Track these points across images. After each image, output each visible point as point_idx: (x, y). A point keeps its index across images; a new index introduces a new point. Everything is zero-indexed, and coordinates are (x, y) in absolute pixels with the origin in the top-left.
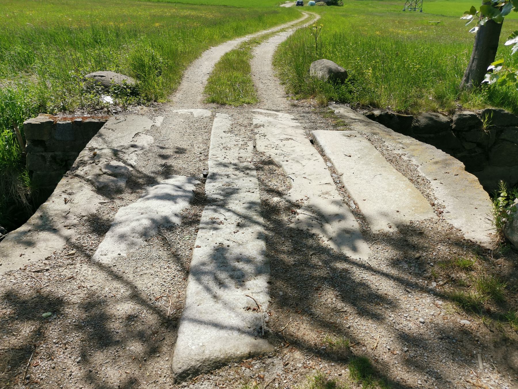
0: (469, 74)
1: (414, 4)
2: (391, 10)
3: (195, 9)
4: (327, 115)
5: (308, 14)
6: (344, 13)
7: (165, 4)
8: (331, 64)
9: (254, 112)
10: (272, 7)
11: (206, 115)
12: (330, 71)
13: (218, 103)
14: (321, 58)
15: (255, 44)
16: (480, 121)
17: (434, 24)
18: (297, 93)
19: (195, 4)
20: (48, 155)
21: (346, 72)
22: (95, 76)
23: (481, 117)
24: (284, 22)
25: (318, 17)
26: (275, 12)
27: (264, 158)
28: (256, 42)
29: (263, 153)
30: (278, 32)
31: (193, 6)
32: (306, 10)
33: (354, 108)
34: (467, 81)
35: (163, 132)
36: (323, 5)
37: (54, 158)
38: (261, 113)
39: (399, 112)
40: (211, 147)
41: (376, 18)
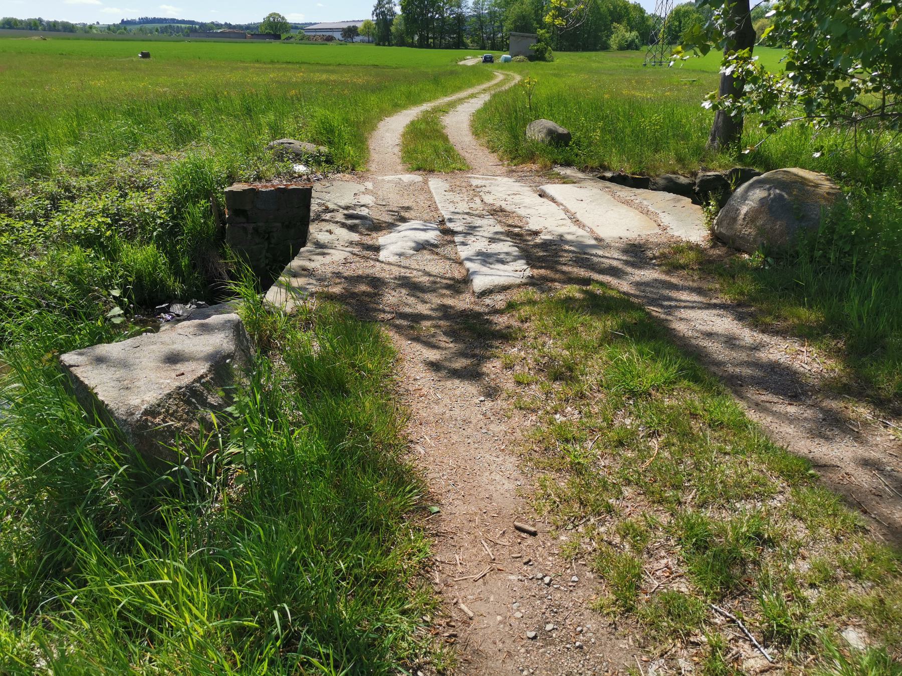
0: (715, 131)
1: (658, 56)
2: (625, 66)
3: (333, 72)
4: (553, 176)
5: (503, 74)
6: (556, 72)
7: (284, 66)
8: (549, 123)
9: (470, 177)
10: (447, 65)
11: (416, 181)
12: (551, 132)
13: (425, 170)
14: (537, 118)
15: (441, 113)
16: (726, 182)
17: (688, 83)
18: (514, 159)
19: (329, 65)
20: (250, 227)
21: (569, 133)
22: (282, 143)
23: (728, 178)
24: (472, 85)
25: (518, 78)
26: (452, 73)
27: (495, 208)
28: (444, 110)
29: (493, 205)
30: (467, 98)
31: (327, 68)
32: (499, 68)
33: (583, 170)
34: (713, 140)
35: (380, 193)
36: (523, 61)
37: (256, 230)
38: (477, 178)
39: (633, 174)
40: (437, 202)
41: (604, 77)
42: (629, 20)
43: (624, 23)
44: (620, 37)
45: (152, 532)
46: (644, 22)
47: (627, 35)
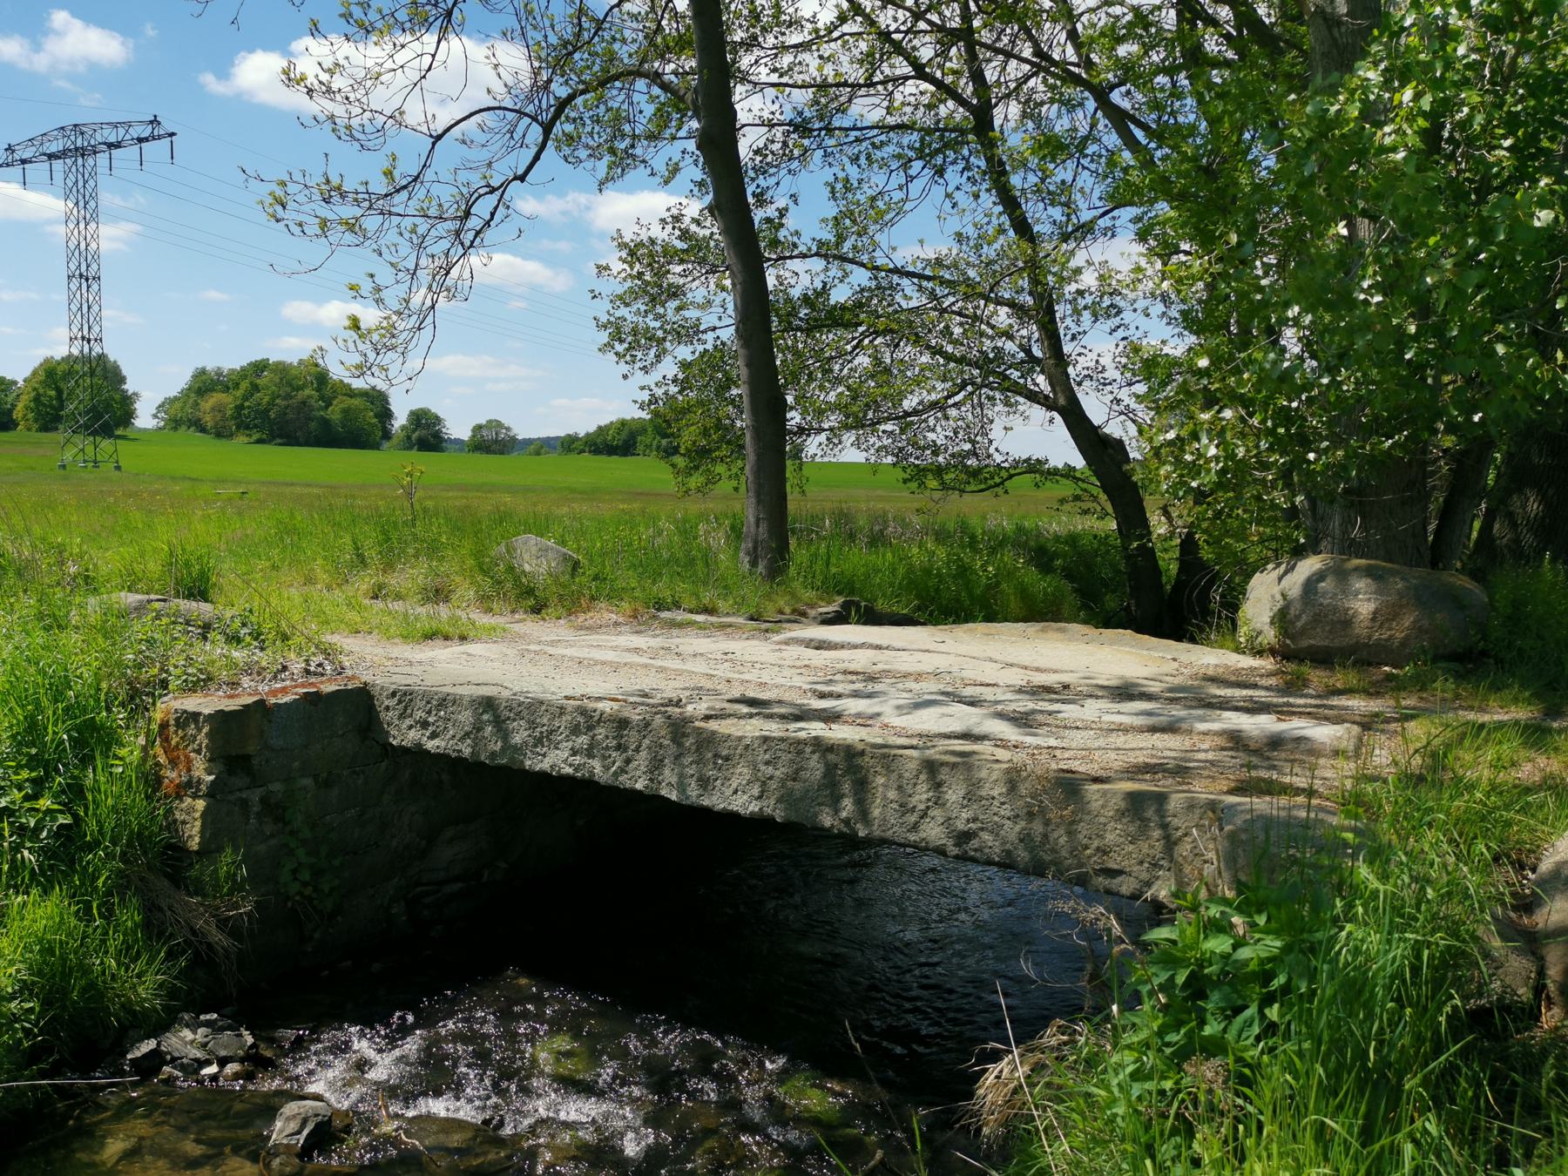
20: (255, 796)
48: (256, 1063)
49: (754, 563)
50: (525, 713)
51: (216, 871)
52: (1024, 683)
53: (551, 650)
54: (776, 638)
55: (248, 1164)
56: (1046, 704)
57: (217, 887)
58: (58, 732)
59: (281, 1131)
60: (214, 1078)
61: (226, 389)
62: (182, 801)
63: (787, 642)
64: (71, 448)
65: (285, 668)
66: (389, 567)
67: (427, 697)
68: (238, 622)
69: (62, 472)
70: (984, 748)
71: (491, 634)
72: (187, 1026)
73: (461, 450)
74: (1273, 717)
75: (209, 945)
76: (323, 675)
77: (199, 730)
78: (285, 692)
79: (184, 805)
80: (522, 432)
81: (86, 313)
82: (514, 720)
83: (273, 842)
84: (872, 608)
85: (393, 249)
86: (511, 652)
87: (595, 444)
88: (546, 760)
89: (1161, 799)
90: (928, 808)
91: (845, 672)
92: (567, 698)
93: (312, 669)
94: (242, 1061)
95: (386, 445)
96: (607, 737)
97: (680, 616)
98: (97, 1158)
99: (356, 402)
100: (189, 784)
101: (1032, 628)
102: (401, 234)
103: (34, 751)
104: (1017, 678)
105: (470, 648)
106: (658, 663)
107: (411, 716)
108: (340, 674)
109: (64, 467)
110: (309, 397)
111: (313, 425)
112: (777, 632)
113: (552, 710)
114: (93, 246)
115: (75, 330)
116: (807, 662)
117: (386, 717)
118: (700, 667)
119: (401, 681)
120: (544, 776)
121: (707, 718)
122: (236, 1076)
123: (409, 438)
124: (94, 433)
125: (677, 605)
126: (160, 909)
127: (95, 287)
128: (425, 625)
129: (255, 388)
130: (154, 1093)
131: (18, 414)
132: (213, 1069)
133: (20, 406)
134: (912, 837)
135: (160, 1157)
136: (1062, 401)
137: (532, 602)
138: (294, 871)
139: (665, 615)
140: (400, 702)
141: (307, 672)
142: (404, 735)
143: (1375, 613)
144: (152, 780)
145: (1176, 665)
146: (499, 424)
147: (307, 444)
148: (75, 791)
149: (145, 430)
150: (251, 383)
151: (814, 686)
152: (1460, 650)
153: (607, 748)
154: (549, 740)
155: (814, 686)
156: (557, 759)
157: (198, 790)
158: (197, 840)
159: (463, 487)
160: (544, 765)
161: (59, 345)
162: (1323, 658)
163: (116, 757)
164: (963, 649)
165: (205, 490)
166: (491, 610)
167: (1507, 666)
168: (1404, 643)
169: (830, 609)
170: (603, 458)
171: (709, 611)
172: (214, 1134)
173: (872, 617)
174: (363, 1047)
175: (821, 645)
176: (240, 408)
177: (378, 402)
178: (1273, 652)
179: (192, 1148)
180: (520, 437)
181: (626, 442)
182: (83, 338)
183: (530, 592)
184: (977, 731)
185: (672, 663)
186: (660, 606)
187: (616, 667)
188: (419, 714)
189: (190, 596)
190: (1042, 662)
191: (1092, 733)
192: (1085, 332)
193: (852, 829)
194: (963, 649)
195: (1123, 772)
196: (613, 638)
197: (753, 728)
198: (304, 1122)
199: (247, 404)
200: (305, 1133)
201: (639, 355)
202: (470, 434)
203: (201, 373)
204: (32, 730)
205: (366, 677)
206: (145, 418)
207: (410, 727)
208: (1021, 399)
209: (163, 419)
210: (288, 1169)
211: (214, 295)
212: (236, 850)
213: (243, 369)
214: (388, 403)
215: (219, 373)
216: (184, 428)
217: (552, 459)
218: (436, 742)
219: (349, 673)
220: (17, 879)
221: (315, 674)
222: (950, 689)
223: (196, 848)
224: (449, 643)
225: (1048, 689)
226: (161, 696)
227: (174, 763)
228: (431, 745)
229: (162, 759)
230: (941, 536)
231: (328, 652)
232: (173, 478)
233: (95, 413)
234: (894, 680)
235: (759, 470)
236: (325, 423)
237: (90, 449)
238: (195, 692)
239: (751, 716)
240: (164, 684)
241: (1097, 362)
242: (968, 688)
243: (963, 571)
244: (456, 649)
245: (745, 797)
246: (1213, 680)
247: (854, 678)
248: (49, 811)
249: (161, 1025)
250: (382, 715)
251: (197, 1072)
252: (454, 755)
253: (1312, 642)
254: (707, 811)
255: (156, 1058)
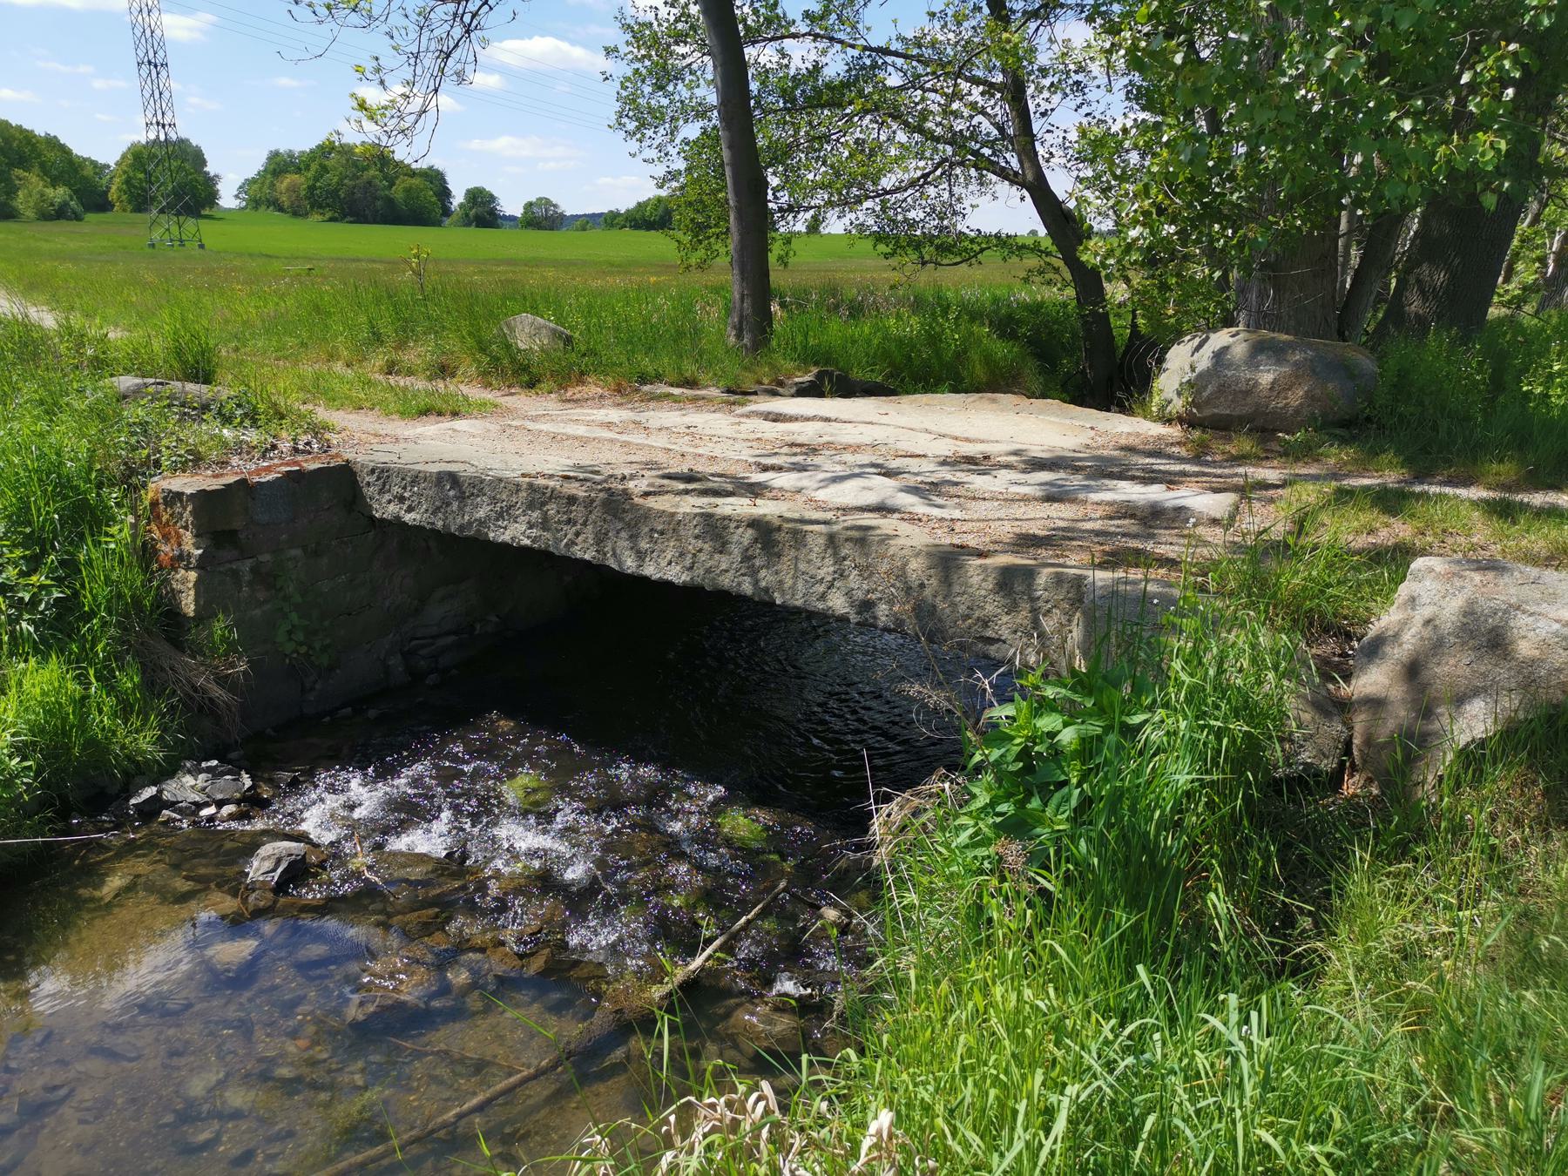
20: (246, 566)
42: (42, 165)
43: (36, 169)
44: (36, 197)
45: (1207, 996)
46: (76, 171)
47: (50, 192)
48: (253, 803)
49: (739, 336)
50: (487, 489)
51: (211, 634)
52: (950, 454)
53: (530, 425)
54: (740, 410)
55: (229, 898)
56: (963, 474)
57: (214, 649)
58: (47, 513)
59: (258, 870)
60: (211, 819)
61: (298, 170)
62: (177, 572)
63: (748, 416)
64: (162, 228)
65: (274, 447)
66: (401, 345)
67: (403, 475)
68: (232, 404)
69: (150, 250)
70: (887, 524)
71: (483, 409)
72: (189, 772)
73: (516, 227)
74: (1163, 487)
75: (211, 699)
76: (310, 453)
77: (185, 509)
78: (266, 471)
79: (178, 576)
80: (569, 207)
81: (157, 97)
82: (478, 496)
83: (267, 607)
84: (846, 377)
85: (403, 32)
86: (494, 427)
87: (635, 219)
88: (507, 532)
89: (1029, 574)
90: (834, 579)
91: (792, 445)
92: (523, 475)
93: (301, 447)
94: (238, 802)
95: (447, 221)
96: (558, 512)
97: (663, 389)
98: (97, 894)
99: (416, 181)
100: (180, 557)
101: (960, 397)
102: (406, 16)
103: (28, 530)
104: (945, 448)
105: (460, 424)
106: (624, 438)
107: (389, 491)
108: (325, 452)
109: (153, 246)
110: (374, 177)
111: (379, 203)
112: (743, 405)
113: (510, 487)
114: (158, 33)
115: (150, 115)
116: (759, 435)
117: (370, 491)
118: (660, 441)
119: (381, 458)
120: (505, 546)
121: (646, 494)
122: (231, 817)
123: (467, 215)
124: (178, 214)
125: (658, 378)
126: (163, 669)
127: (163, 73)
128: (424, 401)
129: (324, 169)
130: (152, 834)
131: (113, 195)
132: (211, 810)
133: (114, 188)
134: (820, 606)
135: (153, 892)
136: (1030, 176)
137: (526, 378)
138: (290, 632)
139: (647, 388)
140: (379, 478)
141: (296, 450)
142: (384, 508)
143: (1273, 383)
144: (146, 553)
145: (1092, 433)
146: (548, 202)
147: (375, 222)
148: (70, 566)
149: (230, 210)
150: (320, 165)
151: (758, 459)
152: (1347, 417)
153: (559, 522)
154: (509, 514)
155: (758, 459)
156: (515, 532)
157: (189, 563)
158: (193, 607)
159: (510, 262)
160: (506, 537)
161: (140, 134)
162: (1222, 426)
163: (107, 534)
164: (903, 421)
165: (277, 265)
166: (491, 385)
167: (1387, 432)
168: (1297, 411)
169: (807, 378)
170: (642, 233)
171: (691, 383)
172: (202, 871)
173: (847, 388)
174: (356, 785)
175: (777, 418)
176: (312, 188)
177: (436, 179)
178: (1181, 420)
179: (182, 885)
180: (568, 214)
181: (662, 217)
182: (158, 123)
183: (525, 369)
184: (890, 502)
185: (637, 438)
186: (643, 379)
187: (584, 442)
188: (396, 490)
189: (195, 378)
190: (971, 434)
191: (996, 504)
192: (1052, 110)
193: (771, 597)
194: (903, 421)
195: (1182, 483)
196: (595, 412)
197: (689, 505)
198: (279, 861)
199: (318, 184)
200: (280, 870)
201: (649, 133)
202: (522, 211)
203: (274, 155)
204: (20, 516)
205: (349, 455)
206: (228, 198)
207: (389, 502)
208: (994, 178)
209: (244, 199)
210: (262, 903)
211: (284, 81)
212: (227, 615)
213: (312, 151)
214: (445, 182)
215: (291, 154)
216: (263, 207)
217: (597, 235)
218: (412, 515)
219: (334, 451)
220: (18, 648)
221: (303, 452)
222: (880, 461)
223: (192, 614)
224: (441, 418)
225: (970, 460)
226: (151, 476)
227: (166, 538)
228: (408, 518)
229: (157, 535)
230: (918, 305)
231: (317, 430)
232: (251, 255)
233: (178, 194)
234: (833, 452)
235: (743, 247)
236: (390, 201)
237: (175, 229)
238: (184, 471)
239: (687, 492)
240: (157, 464)
241: (1064, 138)
242: (898, 460)
243: (934, 339)
244: (446, 424)
245: (678, 568)
246: (1131, 449)
247: (799, 450)
248: (42, 587)
249: (168, 771)
250: (365, 490)
251: (195, 813)
252: (428, 527)
253: (1216, 411)
254: (645, 580)
255: (157, 803)
